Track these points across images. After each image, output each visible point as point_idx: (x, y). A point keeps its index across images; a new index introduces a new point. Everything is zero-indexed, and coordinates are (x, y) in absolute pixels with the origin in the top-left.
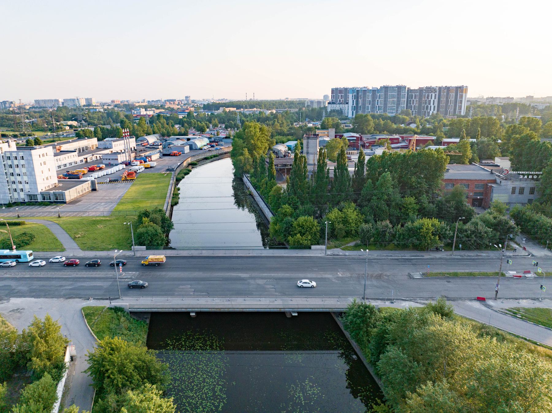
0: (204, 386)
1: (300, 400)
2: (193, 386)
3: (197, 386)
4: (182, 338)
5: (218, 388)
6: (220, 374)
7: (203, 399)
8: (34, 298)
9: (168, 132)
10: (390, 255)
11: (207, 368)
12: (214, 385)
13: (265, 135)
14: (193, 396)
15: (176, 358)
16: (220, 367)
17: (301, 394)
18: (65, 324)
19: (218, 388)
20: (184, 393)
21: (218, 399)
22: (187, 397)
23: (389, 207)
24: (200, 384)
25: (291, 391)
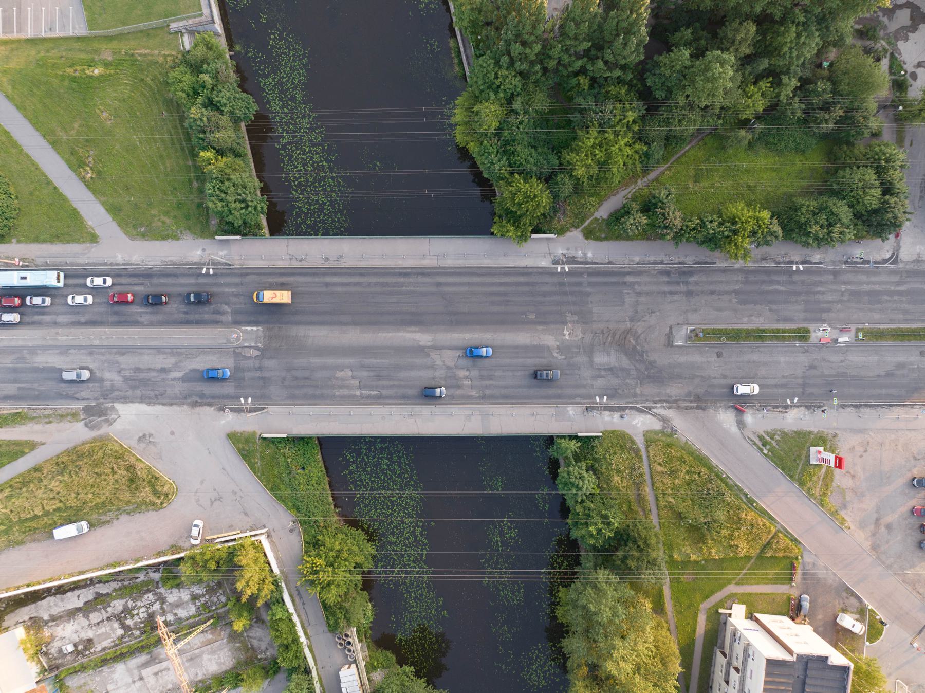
0: (404, 529)
1: (498, 546)
2: (393, 529)
3: (397, 527)
4: (361, 448)
5: (418, 532)
6: (417, 511)
7: (406, 545)
8: (149, 404)
9: (158, 399)
10: (658, 259)
11: (402, 501)
12: (413, 527)
13: (416, 537)
14: (396, 542)
15: (365, 486)
16: (415, 501)
17: (499, 539)
18: (224, 469)
19: (418, 532)
20: (387, 538)
21: (420, 545)
22: (391, 543)
23: (703, 109)
24: (400, 525)
25: (489, 534)
